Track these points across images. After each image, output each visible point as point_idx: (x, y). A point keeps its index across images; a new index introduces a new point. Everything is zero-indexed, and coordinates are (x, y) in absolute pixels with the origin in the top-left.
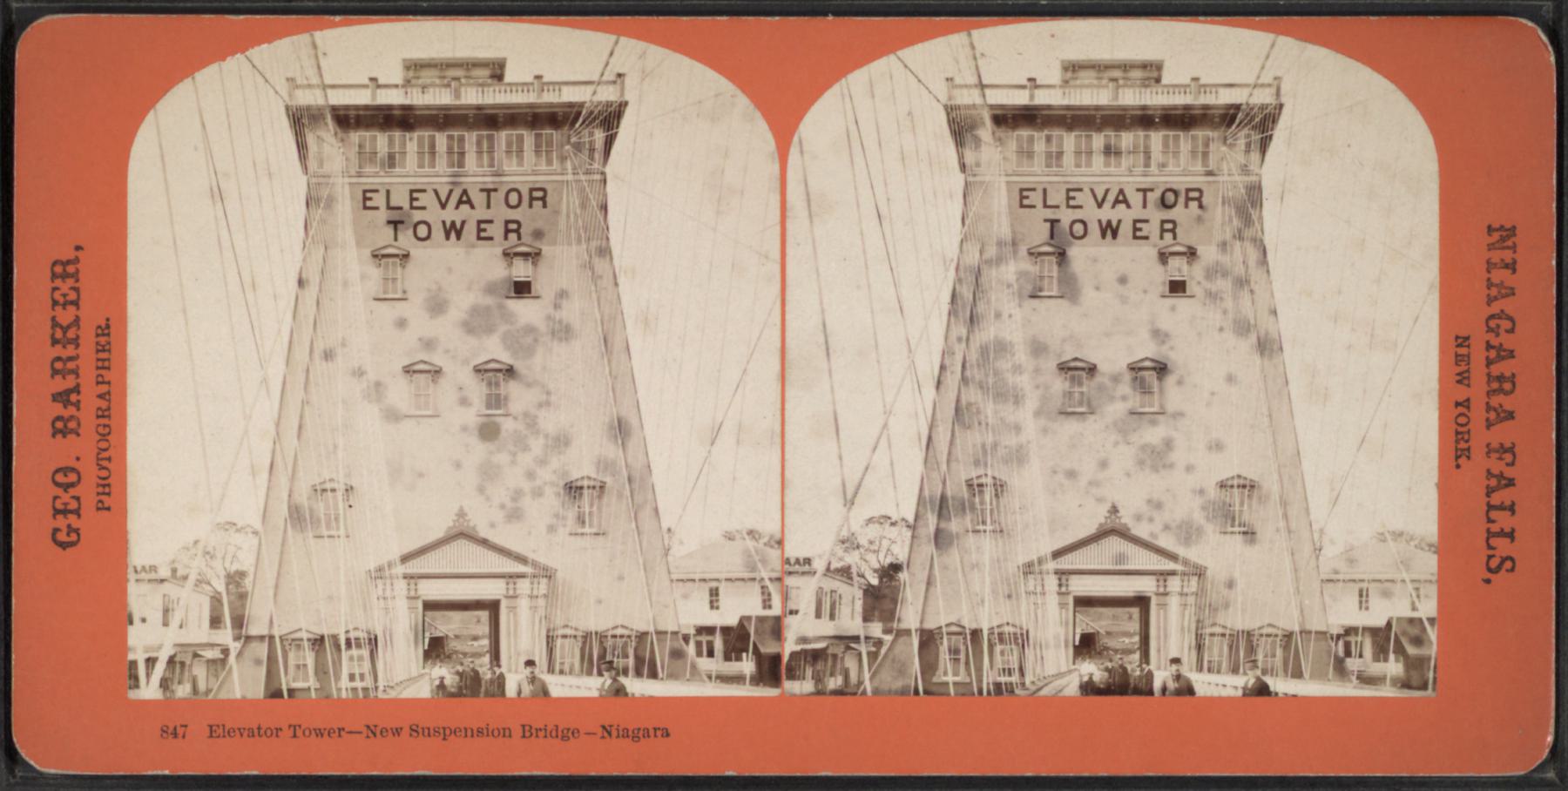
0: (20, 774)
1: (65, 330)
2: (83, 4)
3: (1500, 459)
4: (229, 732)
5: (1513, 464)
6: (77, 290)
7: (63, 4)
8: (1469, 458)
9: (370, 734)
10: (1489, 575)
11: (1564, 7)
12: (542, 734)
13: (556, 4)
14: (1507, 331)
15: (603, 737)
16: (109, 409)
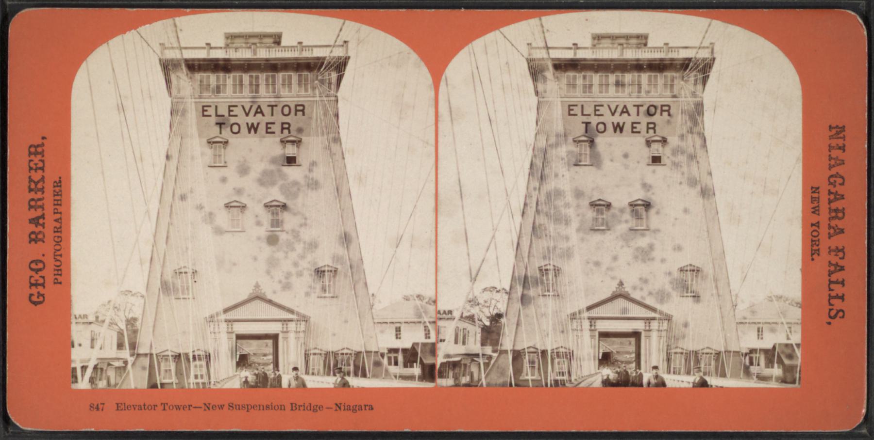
0: (11, 431)
1: (36, 183)
2: (47, 2)
3: (836, 255)
4: (127, 407)
5: (843, 258)
6: (43, 161)
7: (35, 2)
8: (819, 255)
9: (206, 409)
10: (830, 320)
11: (872, 4)
12: (302, 408)
13: (310, 2)
14: (840, 184)
15: (336, 410)
16: (61, 227)
